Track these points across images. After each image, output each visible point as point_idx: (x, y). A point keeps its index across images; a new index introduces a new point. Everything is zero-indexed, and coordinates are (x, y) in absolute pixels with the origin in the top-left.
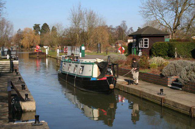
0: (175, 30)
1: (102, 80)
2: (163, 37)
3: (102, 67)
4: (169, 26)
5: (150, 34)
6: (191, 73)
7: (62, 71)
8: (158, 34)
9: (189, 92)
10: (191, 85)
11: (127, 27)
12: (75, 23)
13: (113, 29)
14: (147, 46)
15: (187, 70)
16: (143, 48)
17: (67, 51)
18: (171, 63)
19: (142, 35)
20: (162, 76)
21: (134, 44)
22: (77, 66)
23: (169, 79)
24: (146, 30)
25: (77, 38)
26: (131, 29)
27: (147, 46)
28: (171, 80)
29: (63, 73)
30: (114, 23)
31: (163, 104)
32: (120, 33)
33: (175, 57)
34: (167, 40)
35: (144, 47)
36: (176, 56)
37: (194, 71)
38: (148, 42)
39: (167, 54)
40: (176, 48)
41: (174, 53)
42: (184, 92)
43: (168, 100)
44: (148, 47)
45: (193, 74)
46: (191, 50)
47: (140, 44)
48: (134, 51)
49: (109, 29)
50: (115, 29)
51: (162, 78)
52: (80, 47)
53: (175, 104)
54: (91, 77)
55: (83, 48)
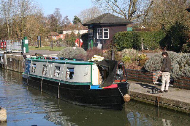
0: (130, 18)
1: (110, 89)
2: (125, 25)
3: (107, 70)
4: (124, 13)
5: (110, 22)
6: (185, 66)
7: (31, 75)
8: (120, 22)
9: (184, 89)
10: (186, 80)
11: (61, 16)
12: (4, 11)
13: (44, 18)
14: (107, 37)
15: (178, 63)
16: (103, 39)
17: (5, 46)
18: (155, 56)
19: (101, 24)
20: (144, 70)
21: (90, 35)
22: (59, 68)
23: (154, 74)
24: (105, 18)
25: (8, 29)
26: (66, 18)
27: (107, 37)
28: (156, 76)
29: (31, 77)
30: (47, 12)
31: (159, 104)
32: (54, 25)
33: (141, 49)
34: (129, 29)
35: (104, 39)
36: (142, 48)
37: (187, 63)
38: (108, 32)
39: (132, 45)
40: (142, 39)
41: (140, 45)
42: (177, 89)
43: (166, 99)
44: (108, 38)
45: (187, 67)
46: (159, 40)
47: (99, 34)
48: (91, 44)
49: (39, 18)
50: (47, 19)
51: (145, 73)
52: (23, 41)
53: (177, 103)
54: (89, 84)
55: (26, 42)
